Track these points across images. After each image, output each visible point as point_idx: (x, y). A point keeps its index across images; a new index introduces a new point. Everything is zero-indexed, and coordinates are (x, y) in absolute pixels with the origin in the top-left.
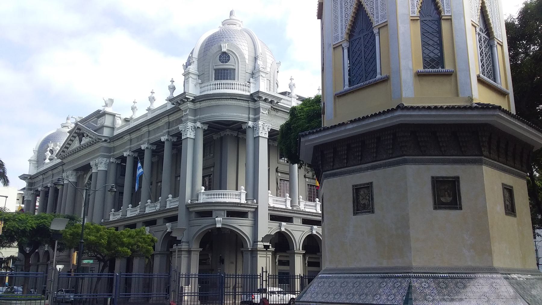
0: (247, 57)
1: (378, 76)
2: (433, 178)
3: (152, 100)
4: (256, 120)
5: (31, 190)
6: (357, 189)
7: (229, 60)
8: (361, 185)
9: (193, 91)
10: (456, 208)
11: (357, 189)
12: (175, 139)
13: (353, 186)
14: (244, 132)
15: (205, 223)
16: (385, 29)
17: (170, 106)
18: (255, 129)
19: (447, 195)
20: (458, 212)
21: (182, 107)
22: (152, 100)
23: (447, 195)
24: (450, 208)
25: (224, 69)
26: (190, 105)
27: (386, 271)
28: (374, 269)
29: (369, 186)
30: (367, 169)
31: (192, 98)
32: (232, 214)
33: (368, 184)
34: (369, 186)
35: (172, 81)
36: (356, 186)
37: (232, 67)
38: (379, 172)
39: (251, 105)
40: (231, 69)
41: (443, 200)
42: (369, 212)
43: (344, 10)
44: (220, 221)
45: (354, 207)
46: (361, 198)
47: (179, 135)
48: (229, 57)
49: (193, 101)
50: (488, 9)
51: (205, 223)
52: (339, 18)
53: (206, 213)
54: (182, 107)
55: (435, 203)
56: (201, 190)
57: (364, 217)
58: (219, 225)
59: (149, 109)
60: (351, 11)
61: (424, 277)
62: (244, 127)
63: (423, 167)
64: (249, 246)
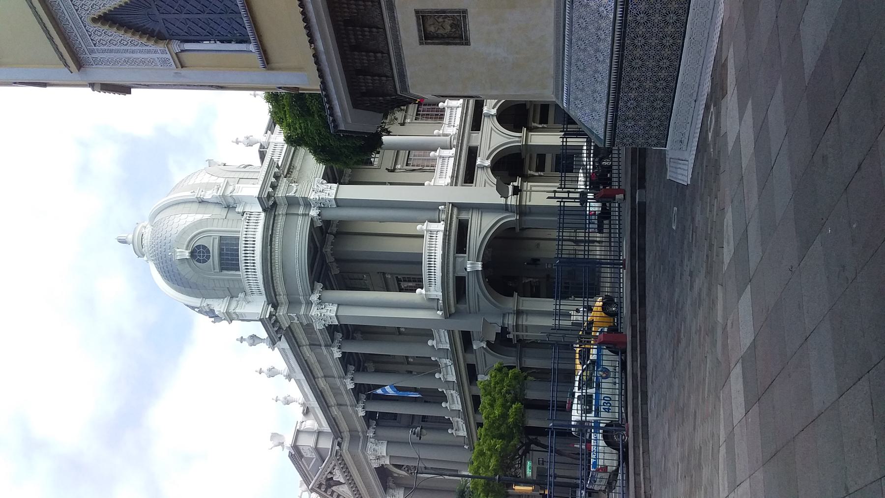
3: (272, 373)
4: (307, 204)
6: (427, 37)
7: (204, 247)
8: (419, 31)
11: (427, 37)
12: (339, 336)
13: (421, 43)
14: (327, 223)
15: (474, 288)
17: (284, 344)
18: (322, 206)
21: (285, 324)
22: (272, 373)
26: (282, 311)
29: (422, 17)
30: (393, 18)
32: (462, 246)
33: (418, 18)
34: (422, 17)
36: (421, 39)
37: (217, 241)
39: (282, 210)
41: (430, 21)
42: (465, 17)
44: (472, 265)
46: (441, 31)
47: (331, 329)
49: (275, 306)
51: (474, 288)
54: (285, 324)
58: (479, 266)
59: (289, 377)
62: (319, 224)
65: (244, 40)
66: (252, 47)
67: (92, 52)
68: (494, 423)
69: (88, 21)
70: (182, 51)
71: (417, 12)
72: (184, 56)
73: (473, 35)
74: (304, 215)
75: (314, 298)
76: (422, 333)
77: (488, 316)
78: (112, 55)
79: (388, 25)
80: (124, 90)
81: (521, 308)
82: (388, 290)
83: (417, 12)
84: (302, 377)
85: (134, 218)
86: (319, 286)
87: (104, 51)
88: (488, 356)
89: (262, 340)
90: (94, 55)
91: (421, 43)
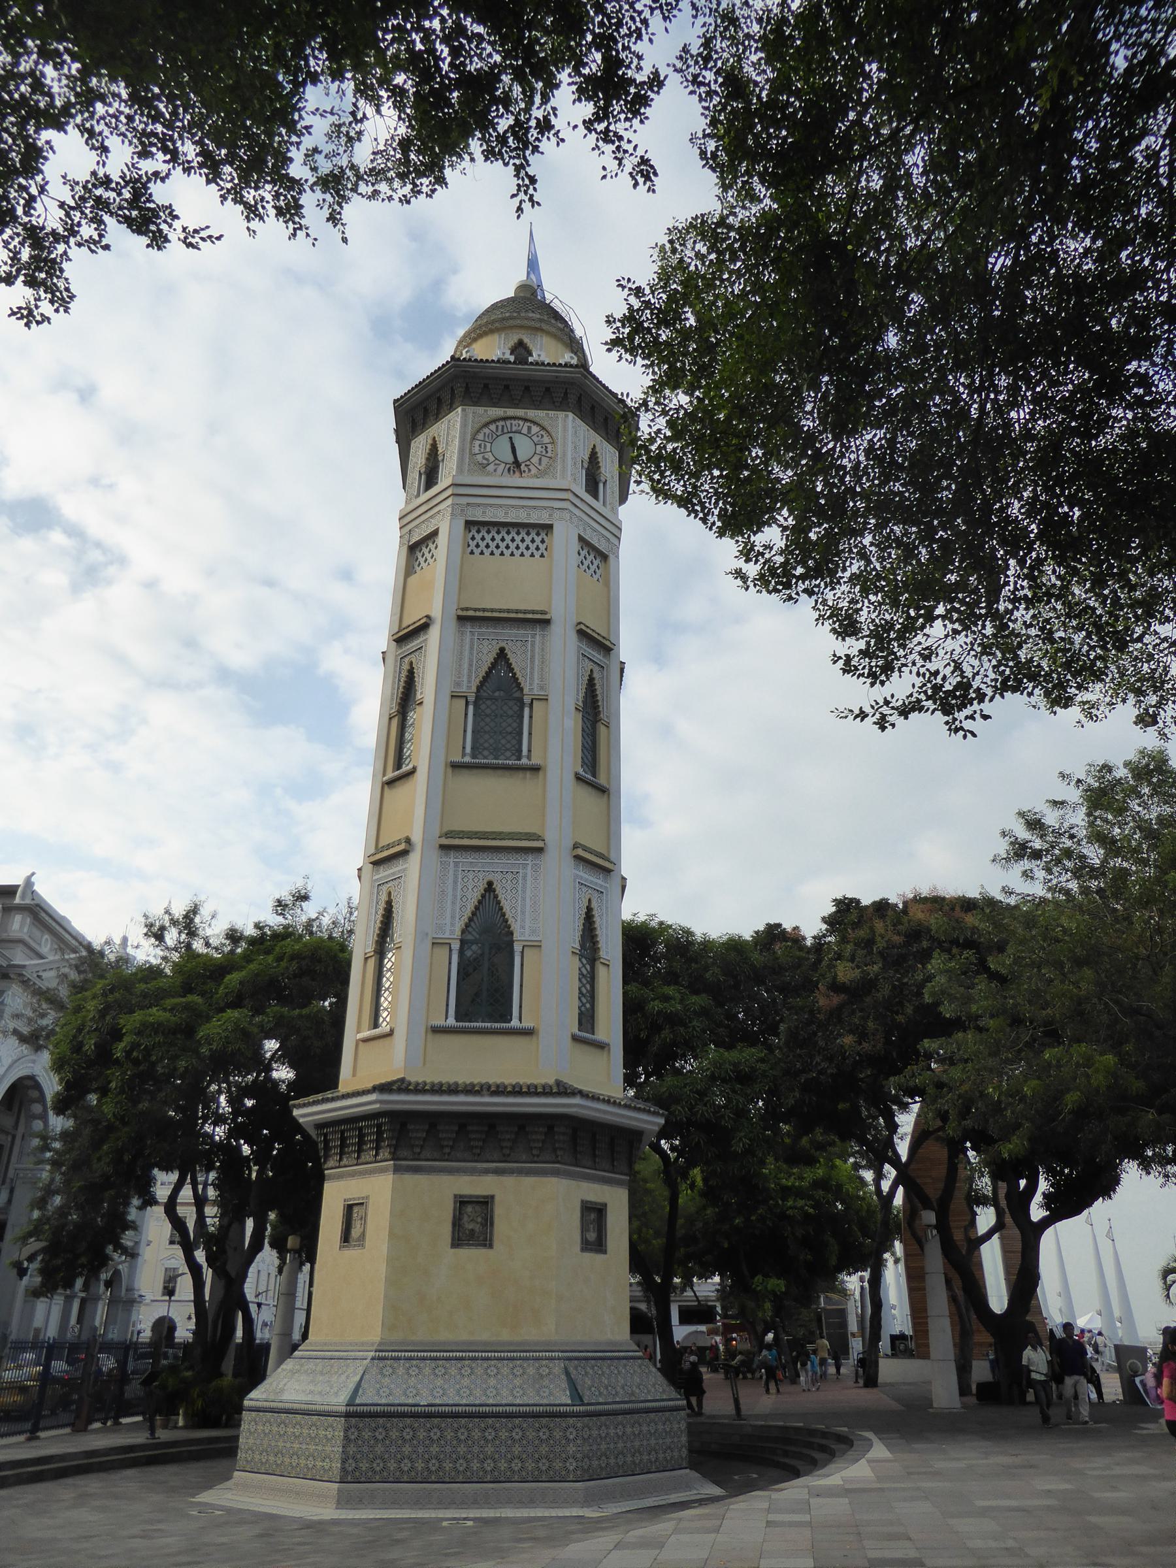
1: (515, 1023)
6: (462, 1202)
8: (471, 1196)
11: (462, 1202)
13: (455, 1196)
16: (535, 950)
20: (602, 1256)
27: (512, 1348)
28: (486, 1343)
29: (486, 1203)
30: (486, 1172)
33: (487, 1197)
34: (486, 1203)
36: (461, 1196)
38: (509, 1181)
42: (485, 1245)
43: (460, 887)
45: (453, 1232)
46: (466, 1218)
50: (597, 919)
52: (450, 897)
55: (453, 1239)
57: (470, 1254)
60: (474, 896)
61: (520, 1359)
63: (573, 1183)
67: (456, 864)
68: (112, 991)
69: (490, 877)
70: (451, 950)
71: (492, 1197)
72: (463, 702)
73: (464, 1252)
78: (467, 647)
79: (479, 1165)
83: (492, 1197)
85: (1044, 712)
87: (456, 876)
90: (452, 864)
91: (455, 1196)
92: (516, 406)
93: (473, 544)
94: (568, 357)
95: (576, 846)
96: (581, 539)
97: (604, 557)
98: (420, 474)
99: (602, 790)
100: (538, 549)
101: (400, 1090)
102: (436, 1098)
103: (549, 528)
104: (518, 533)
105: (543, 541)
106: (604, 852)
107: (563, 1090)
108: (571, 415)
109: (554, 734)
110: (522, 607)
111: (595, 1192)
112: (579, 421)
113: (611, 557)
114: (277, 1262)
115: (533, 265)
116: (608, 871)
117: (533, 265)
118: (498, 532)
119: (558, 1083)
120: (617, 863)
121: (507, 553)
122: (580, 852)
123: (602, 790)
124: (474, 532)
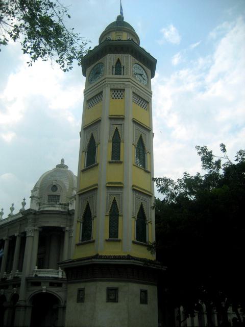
0: (68, 188)
1: (92, 240)
2: (107, 288)
3: (12, 209)
4: (71, 226)
5: (37, 3)
6: (142, 291)
7: (57, 190)
9: (36, 208)
10: (116, 302)
11: (142, 291)
12: (23, 235)
14: (64, 233)
15: (36, 290)
17: (21, 216)
18: (70, 231)
19: (112, 295)
21: (28, 217)
22: (12, 209)
23: (112, 295)
24: (114, 302)
25: (56, 195)
26: (31, 216)
31: (33, 212)
32: (52, 284)
35: (24, 200)
37: (58, 194)
39: (69, 217)
40: (57, 196)
41: (111, 298)
44: (44, 288)
47: (25, 233)
48: (57, 188)
49: (35, 214)
51: (36, 290)
53: (35, 282)
54: (28, 217)
55: (107, 299)
56: (35, 268)
58: (44, 291)
59: (9, 215)
62: (63, 230)
64: (62, 304)
65: (82, 240)
66: (81, 242)
74: (67, 225)
75: (36, 228)
76: (20, 267)
77: (24, 294)
80: (153, 134)
81: (27, 308)
82: (38, 254)
84: (9, 220)
86: (41, 230)
88: (10, 294)
89: (23, 206)
92: (144, 65)
93: (113, 96)
94: (131, 37)
95: (133, 186)
96: (133, 92)
97: (148, 103)
98: (113, 67)
99: (149, 172)
100: (120, 96)
101: (128, 259)
102: (105, 260)
103: (124, 90)
104: (118, 92)
105: (122, 94)
106: (149, 190)
107: (129, 257)
108: (129, 55)
109: (129, 151)
110: (118, 114)
111: (145, 287)
112: (132, 57)
113: (150, 103)
114: (68, 303)
115: (121, 13)
116: (151, 196)
117: (121, 13)
118: (115, 92)
119: (128, 255)
120: (153, 194)
121: (114, 98)
122: (135, 188)
123: (149, 172)
124: (113, 92)
